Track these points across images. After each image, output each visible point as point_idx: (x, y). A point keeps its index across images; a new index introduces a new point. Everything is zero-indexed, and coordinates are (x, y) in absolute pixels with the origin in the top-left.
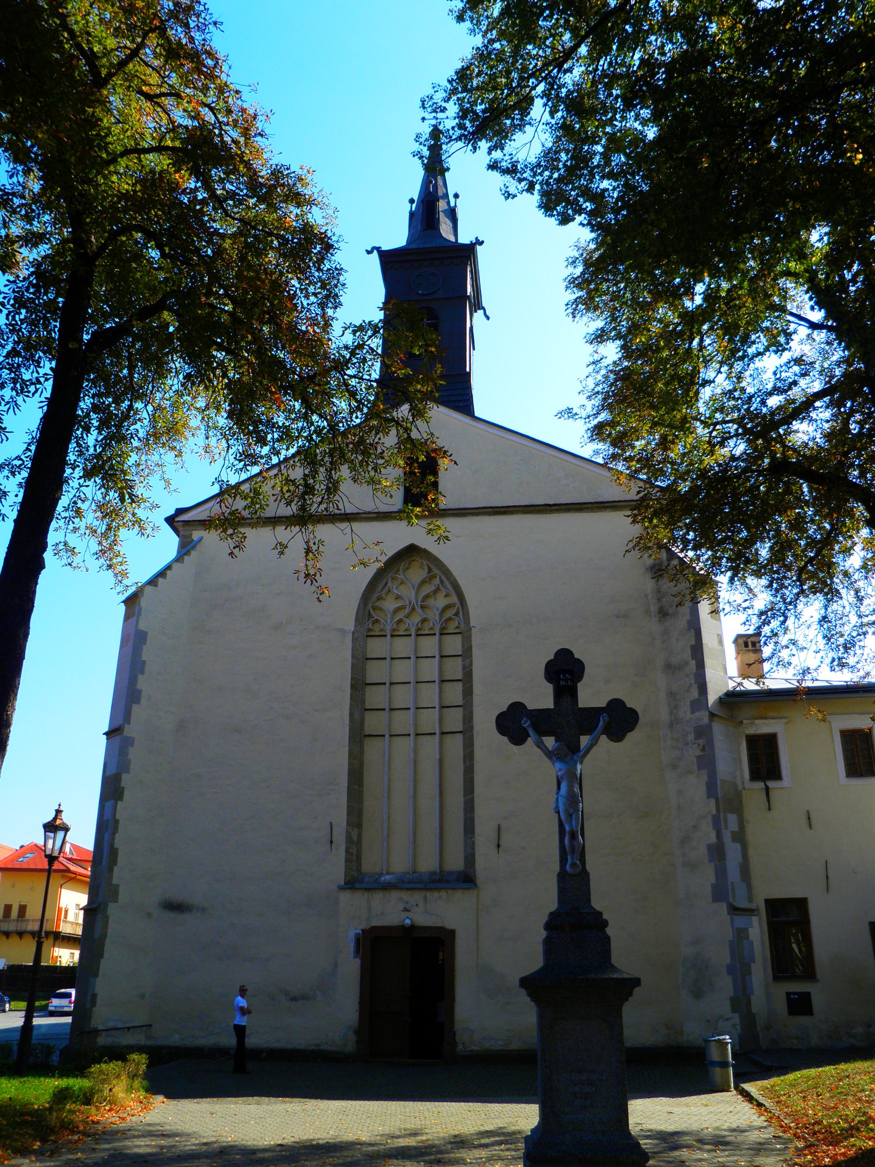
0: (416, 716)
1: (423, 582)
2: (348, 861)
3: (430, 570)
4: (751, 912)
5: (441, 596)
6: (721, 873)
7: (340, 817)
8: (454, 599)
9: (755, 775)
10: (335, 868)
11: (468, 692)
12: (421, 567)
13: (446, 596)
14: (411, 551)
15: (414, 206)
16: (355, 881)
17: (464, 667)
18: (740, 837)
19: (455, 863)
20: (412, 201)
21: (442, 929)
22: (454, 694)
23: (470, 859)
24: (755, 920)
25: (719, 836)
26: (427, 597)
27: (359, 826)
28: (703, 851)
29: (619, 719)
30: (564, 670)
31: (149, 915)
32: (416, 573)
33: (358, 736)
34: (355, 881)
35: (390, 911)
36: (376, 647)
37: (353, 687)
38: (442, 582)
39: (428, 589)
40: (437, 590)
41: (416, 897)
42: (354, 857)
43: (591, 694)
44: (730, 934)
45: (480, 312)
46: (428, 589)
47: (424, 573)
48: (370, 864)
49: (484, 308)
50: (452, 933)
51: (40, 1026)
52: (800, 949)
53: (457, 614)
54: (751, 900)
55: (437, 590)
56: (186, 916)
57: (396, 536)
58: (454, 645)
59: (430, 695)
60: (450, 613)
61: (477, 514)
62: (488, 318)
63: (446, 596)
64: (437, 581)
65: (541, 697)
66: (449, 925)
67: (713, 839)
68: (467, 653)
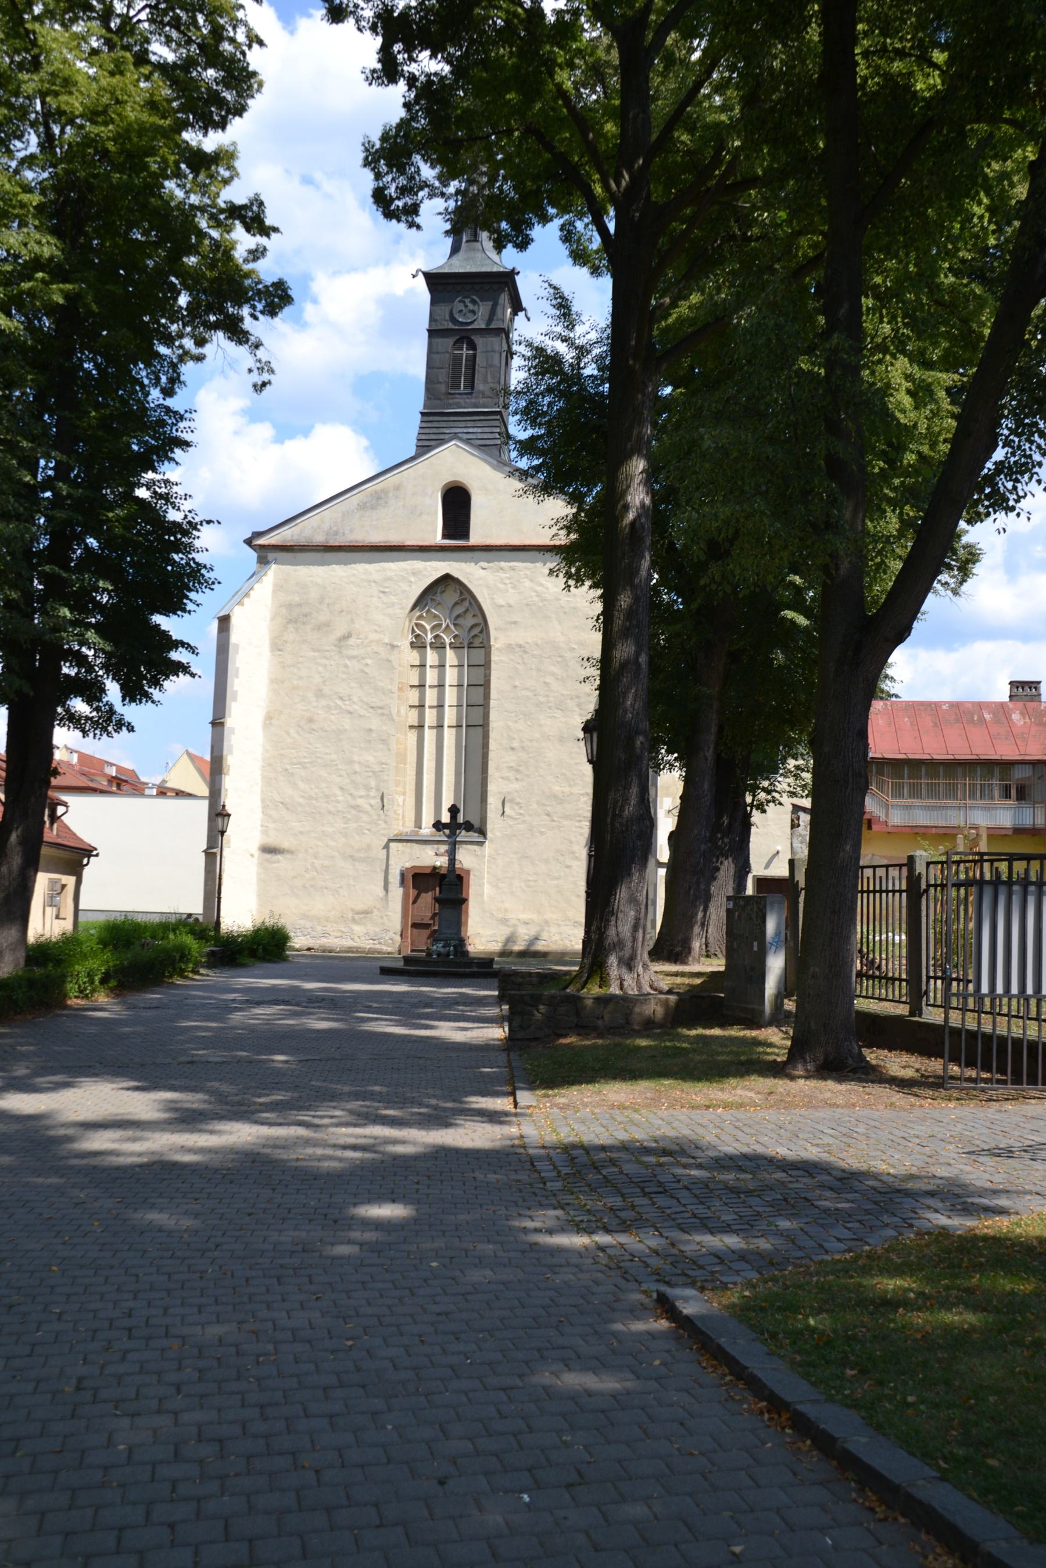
1: (456, 604)
3: (461, 593)
5: (469, 615)
8: (479, 620)
12: (455, 591)
13: (474, 616)
14: (447, 579)
23: (124, 1328)
26: (458, 616)
31: (252, 855)
32: (451, 596)
38: (470, 603)
39: (459, 610)
40: (467, 610)
43: (461, 819)
45: (521, 314)
46: (459, 610)
47: (456, 597)
49: (525, 309)
51: (494, 990)
52: (30, 1044)
53: (481, 632)
55: (467, 610)
56: (279, 857)
57: (434, 569)
60: (476, 631)
61: (500, 550)
62: (529, 320)
63: (474, 616)
64: (466, 604)
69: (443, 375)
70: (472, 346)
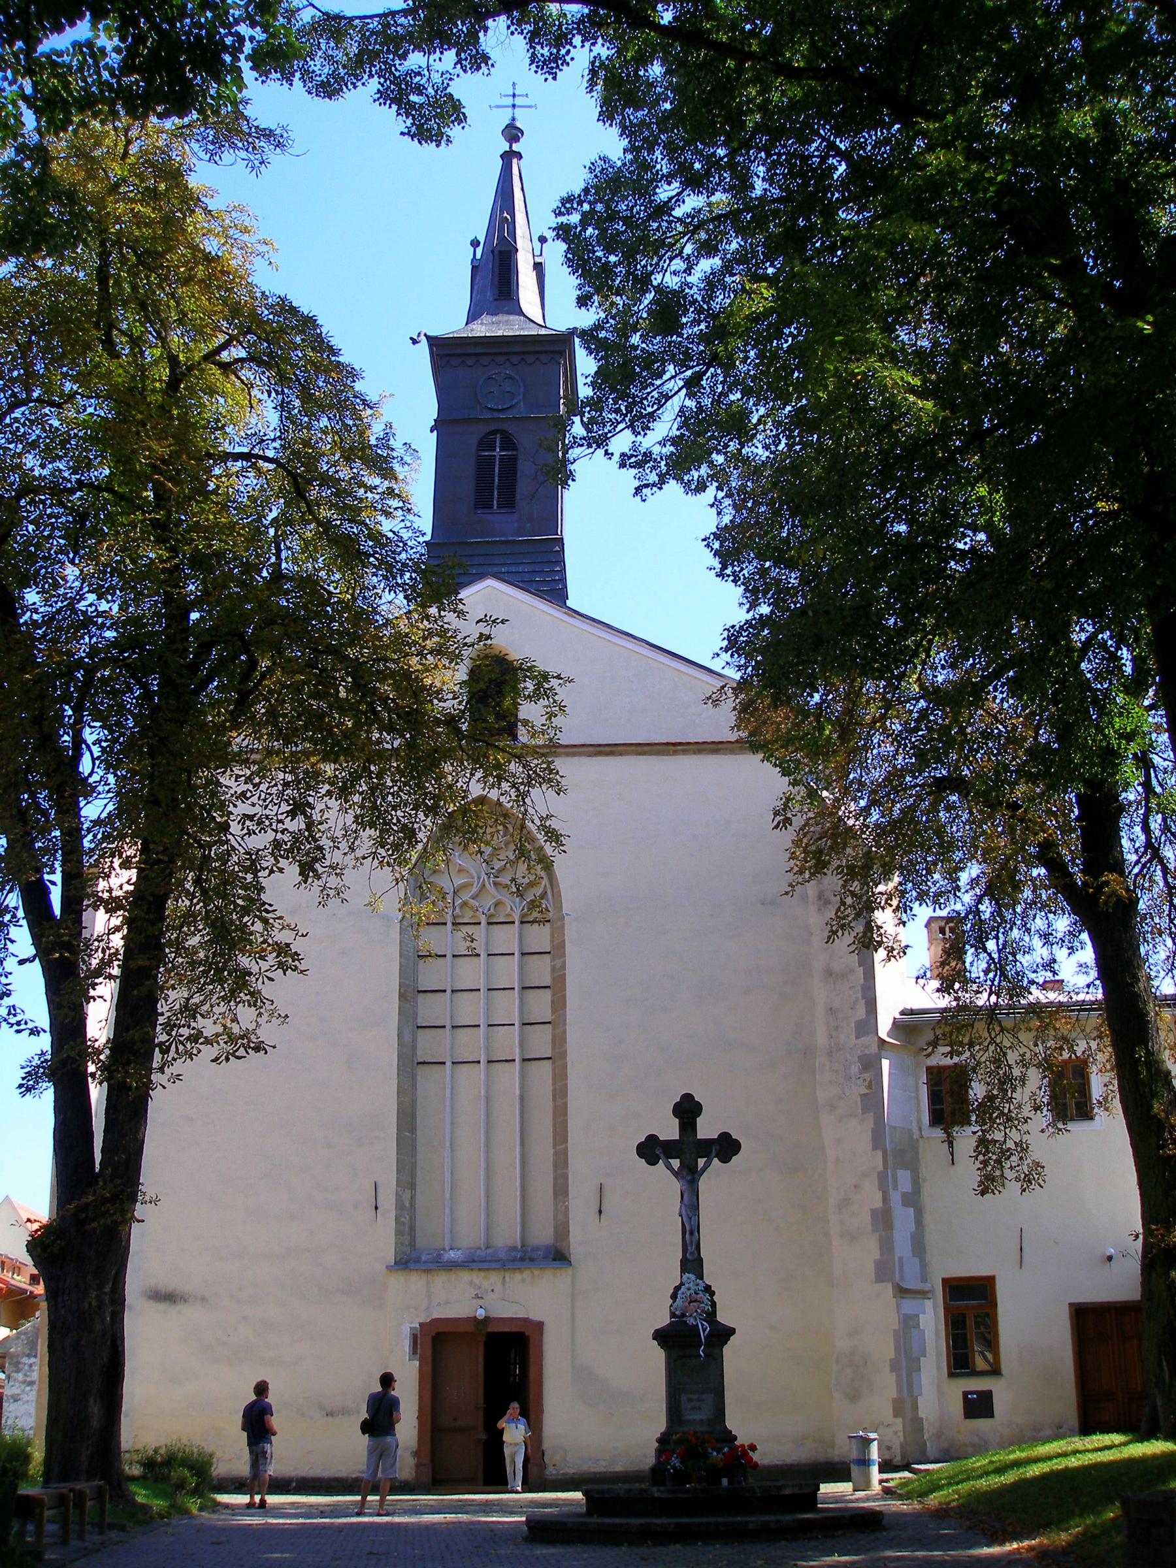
0: (488, 1038)
2: (398, 1233)
4: (924, 1294)
6: (887, 1245)
7: (389, 1179)
9: (937, 1118)
10: (383, 1241)
11: (559, 1004)
15: (479, 250)
16: (409, 1259)
17: (553, 969)
18: (913, 1200)
19: (543, 1235)
20: (475, 243)
21: (526, 1320)
22: (541, 1006)
24: (928, 1304)
25: (885, 1198)
27: (413, 1186)
28: (867, 1216)
29: (726, 1147)
30: (687, 1110)
33: (411, 1064)
34: (409, 1259)
35: (459, 1298)
36: (433, 940)
37: (402, 997)
41: (491, 1280)
42: (407, 1229)
43: (706, 1129)
44: (894, 1322)
48: (430, 1234)
50: (540, 1326)
54: (924, 1279)
58: (540, 937)
59: (508, 1007)
65: (670, 1130)
66: (535, 1316)
67: (878, 1203)
68: (557, 951)
69: (466, 488)
70: (509, 443)
